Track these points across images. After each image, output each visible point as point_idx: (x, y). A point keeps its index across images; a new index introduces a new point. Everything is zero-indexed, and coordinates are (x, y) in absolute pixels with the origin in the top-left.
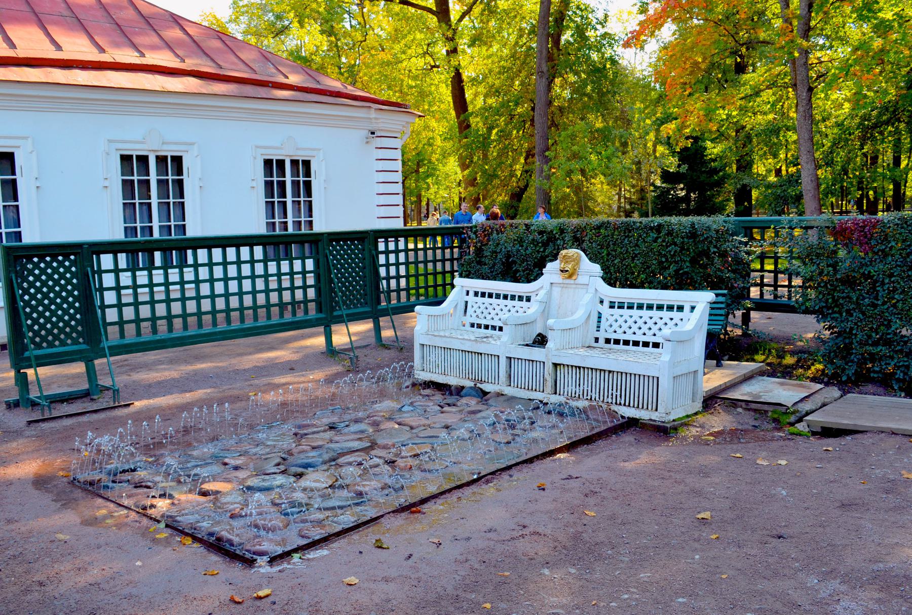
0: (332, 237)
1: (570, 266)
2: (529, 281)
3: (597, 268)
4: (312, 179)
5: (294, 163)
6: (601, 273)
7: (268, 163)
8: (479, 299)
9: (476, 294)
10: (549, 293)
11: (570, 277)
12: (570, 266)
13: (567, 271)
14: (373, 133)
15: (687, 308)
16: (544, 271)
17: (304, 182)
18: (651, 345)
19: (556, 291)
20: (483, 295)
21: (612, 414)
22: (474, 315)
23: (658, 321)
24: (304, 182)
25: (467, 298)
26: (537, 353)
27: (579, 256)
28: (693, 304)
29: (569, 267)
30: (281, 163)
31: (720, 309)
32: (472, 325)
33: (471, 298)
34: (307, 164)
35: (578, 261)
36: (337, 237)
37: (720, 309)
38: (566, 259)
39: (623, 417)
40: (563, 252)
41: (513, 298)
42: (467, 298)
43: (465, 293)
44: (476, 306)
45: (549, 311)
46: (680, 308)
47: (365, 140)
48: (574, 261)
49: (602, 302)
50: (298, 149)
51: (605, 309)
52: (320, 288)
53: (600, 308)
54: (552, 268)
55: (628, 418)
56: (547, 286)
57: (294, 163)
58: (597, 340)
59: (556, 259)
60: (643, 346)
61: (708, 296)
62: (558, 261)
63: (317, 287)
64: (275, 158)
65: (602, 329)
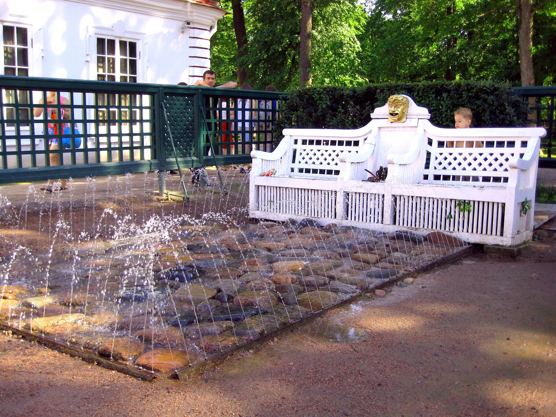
0: (166, 91)
1: (400, 110)
2: (355, 127)
3: (424, 112)
4: (137, 58)
5: (123, 44)
6: (428, 116)
7: (101, 41)
8: (308, 147)
9: (304, 142)
10: (378, 136)
11: (399, 119)
12: (400, 110)
13: (397, 114)
14: (188, 23)
15: (518, 144)
16: (372, 115)
17: (130, 60)
18: (481, 179)
19: (383, 133)
20: (311, 142)
21: (453, 241)
22: (303, 162)
23: (332, 153)
24: (130, 60)
25: (295, 146)
26: (377, 188)
27: (407, 100)
28: (524, 140)
29: (399, 111)
30: (112, 43)
31: (415, 225)
32: (301, 171)
33: (299, 147)
34: (133, 46)
35: (406, 105)
36: (169, 91)
37: (415, 225)
38: (396, 104)
39: (469, 243)
40: (393, 97)
41: (341, 143)
42: (295, 146)
43: (293, 142)
44: (304, 154)
45: (377, 154)
46: (511, 144)
47: (181, 30)
48: (403, 104)
49: (430, 143)
50: (126, 32)
51: (435, 150)
52: (155, 137)
53: (430, 149)
54: (380, 112)
55: (472, 244)
56: (375, 131)
57: (123, 44)
58: (292, 170)
59: (383, 105)
60: (320, 173)
61: (542, 131)
62: (387, 105)
63: (152, 134)
64: (107, 38)
65: (431, 165)
